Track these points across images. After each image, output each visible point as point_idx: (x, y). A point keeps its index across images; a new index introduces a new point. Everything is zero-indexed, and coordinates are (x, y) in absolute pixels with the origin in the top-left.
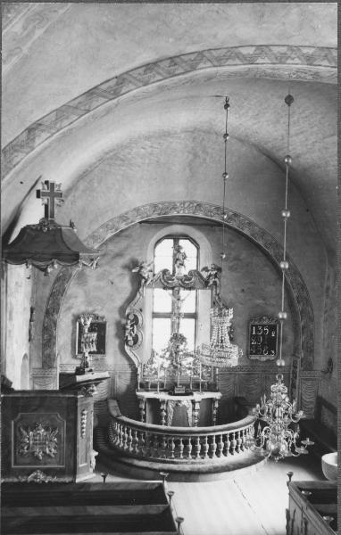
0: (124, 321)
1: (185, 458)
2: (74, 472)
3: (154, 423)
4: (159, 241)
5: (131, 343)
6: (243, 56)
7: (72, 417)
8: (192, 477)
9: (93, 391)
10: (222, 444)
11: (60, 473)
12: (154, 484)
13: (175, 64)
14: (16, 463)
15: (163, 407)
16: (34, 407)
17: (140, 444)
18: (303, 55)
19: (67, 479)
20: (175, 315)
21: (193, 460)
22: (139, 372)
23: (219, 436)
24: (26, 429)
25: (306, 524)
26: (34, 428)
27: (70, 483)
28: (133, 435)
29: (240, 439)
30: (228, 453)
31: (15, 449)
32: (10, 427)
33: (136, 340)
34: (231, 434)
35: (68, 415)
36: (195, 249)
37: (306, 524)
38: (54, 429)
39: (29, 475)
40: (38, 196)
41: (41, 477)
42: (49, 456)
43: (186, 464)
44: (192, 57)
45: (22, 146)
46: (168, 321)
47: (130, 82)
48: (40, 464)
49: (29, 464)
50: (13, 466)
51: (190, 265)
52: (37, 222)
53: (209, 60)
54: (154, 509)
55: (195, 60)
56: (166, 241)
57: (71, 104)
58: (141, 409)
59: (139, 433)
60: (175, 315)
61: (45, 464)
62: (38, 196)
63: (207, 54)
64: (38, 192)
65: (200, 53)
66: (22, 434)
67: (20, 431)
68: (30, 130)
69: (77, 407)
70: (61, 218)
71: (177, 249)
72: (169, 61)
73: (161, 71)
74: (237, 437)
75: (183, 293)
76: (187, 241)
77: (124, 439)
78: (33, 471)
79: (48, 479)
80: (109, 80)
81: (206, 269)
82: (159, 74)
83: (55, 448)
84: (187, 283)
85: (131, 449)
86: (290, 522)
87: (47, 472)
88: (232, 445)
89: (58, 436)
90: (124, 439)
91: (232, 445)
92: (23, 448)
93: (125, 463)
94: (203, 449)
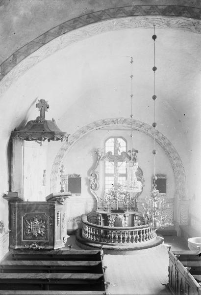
0: (89, 178)
1: (119, 243)
2: (53, 244)
3: (105, 225)
4: (106, 140)
5: (94, 187)
6: (127, 12)
7: (52, 215)
8: (122, 252)
9: (62, 201)
10: (145, 234)
11: (47, 244)
12: (96, 251)
13: (90, 18)
14: (24, 239)
15: (109, 218)
16: (33, 210)
17: (97, 236)
18: (159, 10)
19: (50, 247)
20: (116, 175)
21: (123, 244)
22: (98, 202)
23: (140, 231)
24: (29, 221)
25: (178, 273)
26: (33, 220)
27: (51, 249)
28: (93, 231)
29: (147, 234)
30: (141, 241)
31: (24, 231)
32: (21, 219)
33: (96, 186)
34: (143, 231)
35: (51, 214)
36: (125, 143)
37: (178, 273)
38: (43, 221)
39: (30, 245)
40: (36, 107)
41: (37, 246)
42: (40, 235)
43: (117, 246)
44: (99, 13)
45: (10, 63)
46: (113, 178)
47: (66, 28)
48: (36, 240)
49: (31, 239)
50: (22, 240)
51: (123, 149)
52: (36, 119)
53: (108, 15)
54: (94, 263)
55: (100, 15)
56: (110, 139)
57: (35, 41)
58: (98, 219)
59: (93, 229)
60: (116, 175)
61: (39, 240)
62: (36, 107)
63: (107, 12)
64: (37, 104)
65: (103, 12)
66: (27, 224)
67: (26, 222)
68: (14, 55)
69: (54, 210)
70: (48, 117)
71: (116, 142)
72: (87, 16)
73: (82, 21)
74: (146, 233)
75: (119, 163)
76: (122, 139)
77: (89, 234)
78: (32, 243)
79: (40, 247)
80: (55, 28)
81: (130, 151)
82: (81, 22)
83: (44, 231)
84: (120, 159)
85: (92, 238)
86: (170, 273)
87: (39, 244)
88: (146, 235)
89: (46, 225)
90: (89, 234)
91: (146, 235)
92: (27, 231)
93: (90, 246)
94: (119, 238)
